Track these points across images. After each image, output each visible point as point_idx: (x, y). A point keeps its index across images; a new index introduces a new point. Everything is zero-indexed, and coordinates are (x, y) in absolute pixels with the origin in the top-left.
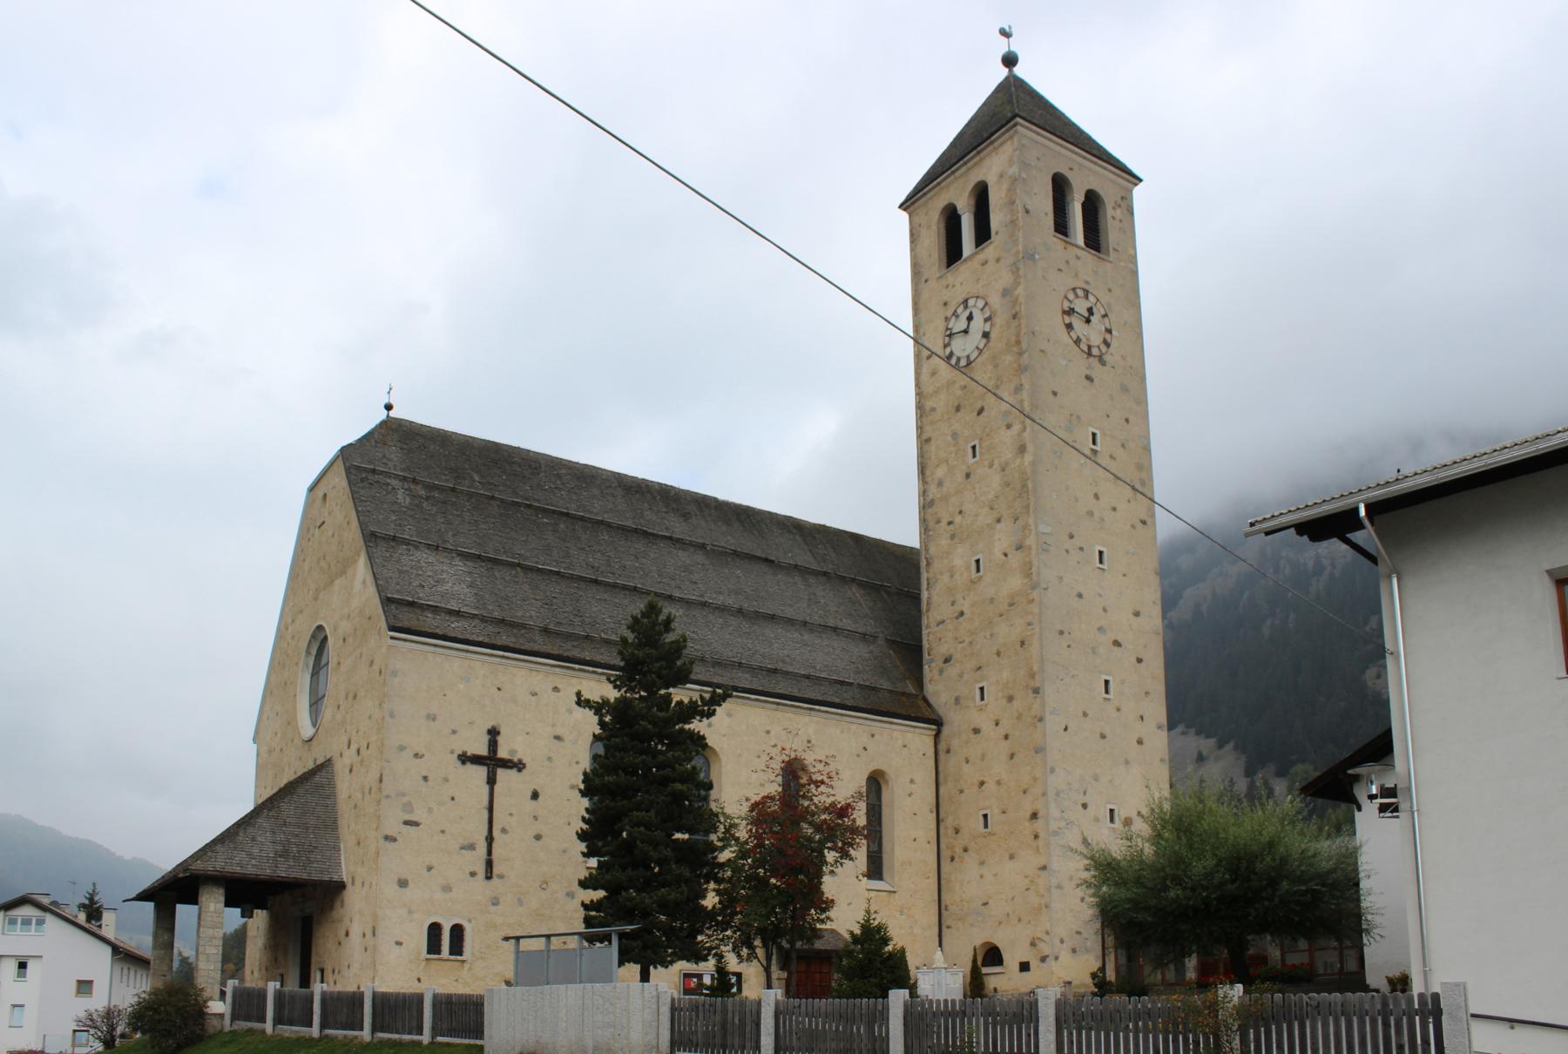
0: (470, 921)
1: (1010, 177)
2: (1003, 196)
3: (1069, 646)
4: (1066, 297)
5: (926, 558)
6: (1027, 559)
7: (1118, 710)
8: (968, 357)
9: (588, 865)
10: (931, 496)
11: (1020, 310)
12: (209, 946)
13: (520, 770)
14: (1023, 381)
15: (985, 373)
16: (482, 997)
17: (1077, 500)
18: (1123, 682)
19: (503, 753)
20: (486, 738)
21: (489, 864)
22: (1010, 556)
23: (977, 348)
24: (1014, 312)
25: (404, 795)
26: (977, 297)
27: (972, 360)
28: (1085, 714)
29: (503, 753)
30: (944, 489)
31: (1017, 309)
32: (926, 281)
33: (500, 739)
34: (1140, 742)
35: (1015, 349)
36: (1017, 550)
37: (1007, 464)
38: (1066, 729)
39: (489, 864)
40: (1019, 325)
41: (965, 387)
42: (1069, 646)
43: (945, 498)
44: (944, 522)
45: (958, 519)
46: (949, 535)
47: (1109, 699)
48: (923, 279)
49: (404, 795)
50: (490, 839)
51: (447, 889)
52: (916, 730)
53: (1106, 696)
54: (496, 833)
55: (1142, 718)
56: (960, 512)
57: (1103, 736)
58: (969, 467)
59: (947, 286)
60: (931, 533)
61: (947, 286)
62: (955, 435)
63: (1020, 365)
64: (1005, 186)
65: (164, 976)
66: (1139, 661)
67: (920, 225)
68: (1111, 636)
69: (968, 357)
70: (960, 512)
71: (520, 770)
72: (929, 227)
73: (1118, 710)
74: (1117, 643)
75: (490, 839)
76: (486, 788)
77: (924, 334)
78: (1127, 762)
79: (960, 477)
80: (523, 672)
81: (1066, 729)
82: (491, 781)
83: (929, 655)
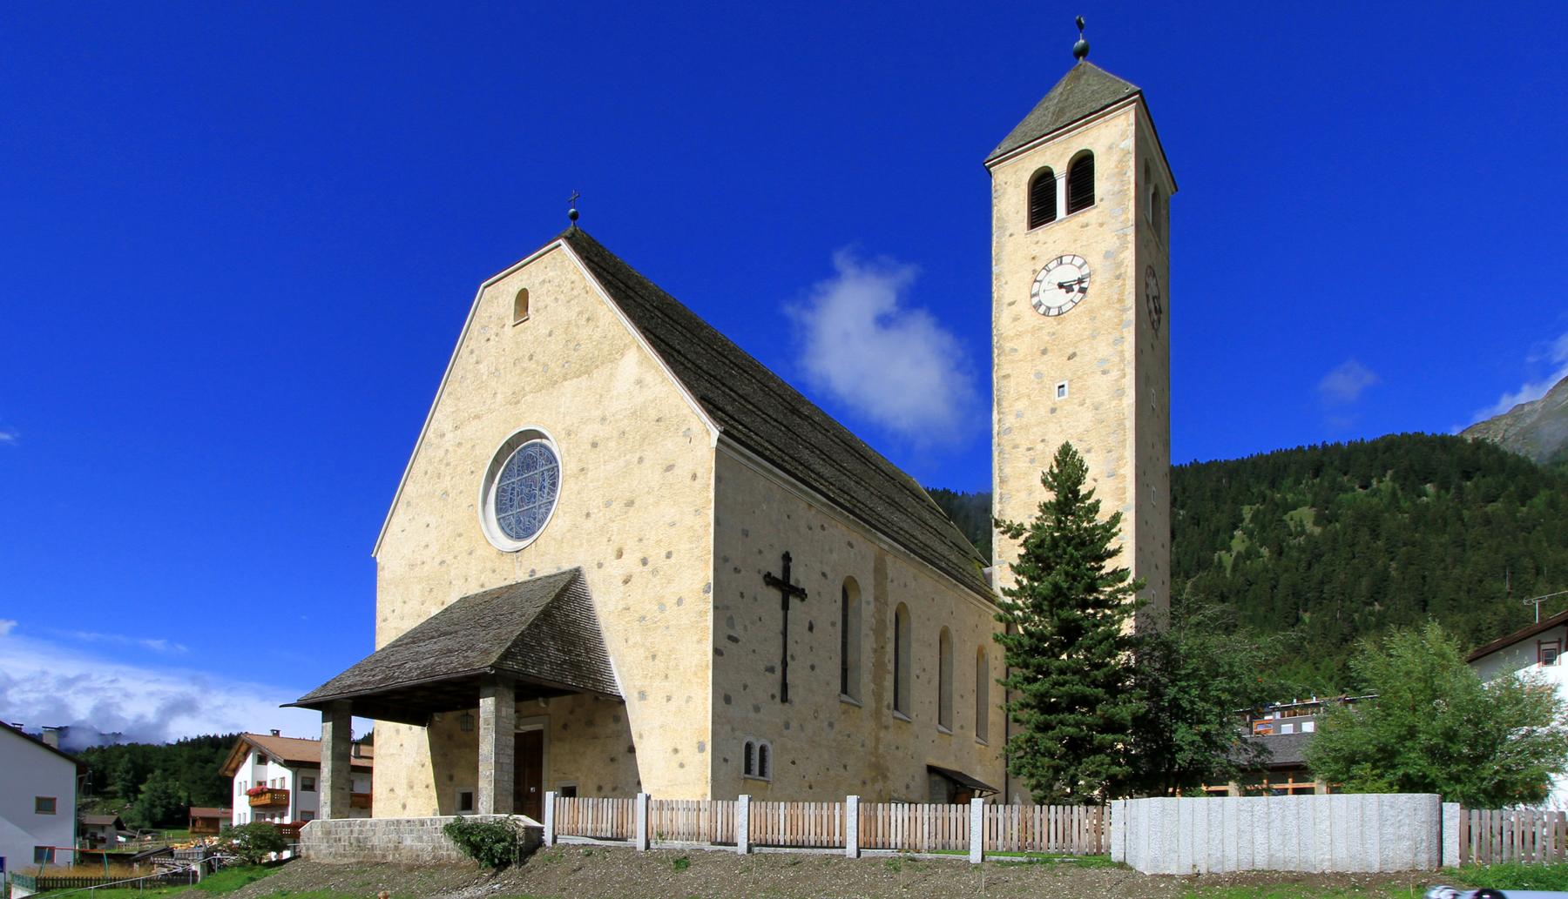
0: (772, 743)
1: (1123, 149)
2: (1113, 166)
5: (1000, 477)
6: (1121, 485)
8: (1049, 308)
9: (842, 699)
10: (1008, 425)
11: (1126, 272)
12: (503, 754)
14: (1125, 334)
15: (1079, 323)
16: (36, 813)
20: (780, 563)
21: (785, 687)
22: (1100, 481)
24: (1118, 273)
25: (728, 608)
26: (1074, 256)
27: (1064, 311)
30: (1024, 420)
31: (1123, 270)
32: (1011, 235)
35: (1117, 306)
36: (1108, 477)
37: (1101, 404)
39: (785, 687)
40: (1124, 285)
41: (1054, 334)
43: (1026, 428)
44: (1022, 449)
45: (1040, 446)
46: (1028, 459)
48: (1008, 233)
49: (728, 608)
50: (785, 664)
51: (757, 709)
54: (788, 659)
56: (1043, 441)
58: (1055, 403)
59: (1037, 242)
60: (1005, 456)
61: (1037, 242)
62: (1039, 375)
63: (1121, 321)
64: (1115, 158)
65: (343, 789)
67: (1006, 183)
69: (1060, 307)
70: (1043, 441)
72: (1017, 186)
75: (785, 664)
76: (780, 614)
77: (1006, 283)
79: (1043, 411)
82: (785, 606)
83: (1000, 556)
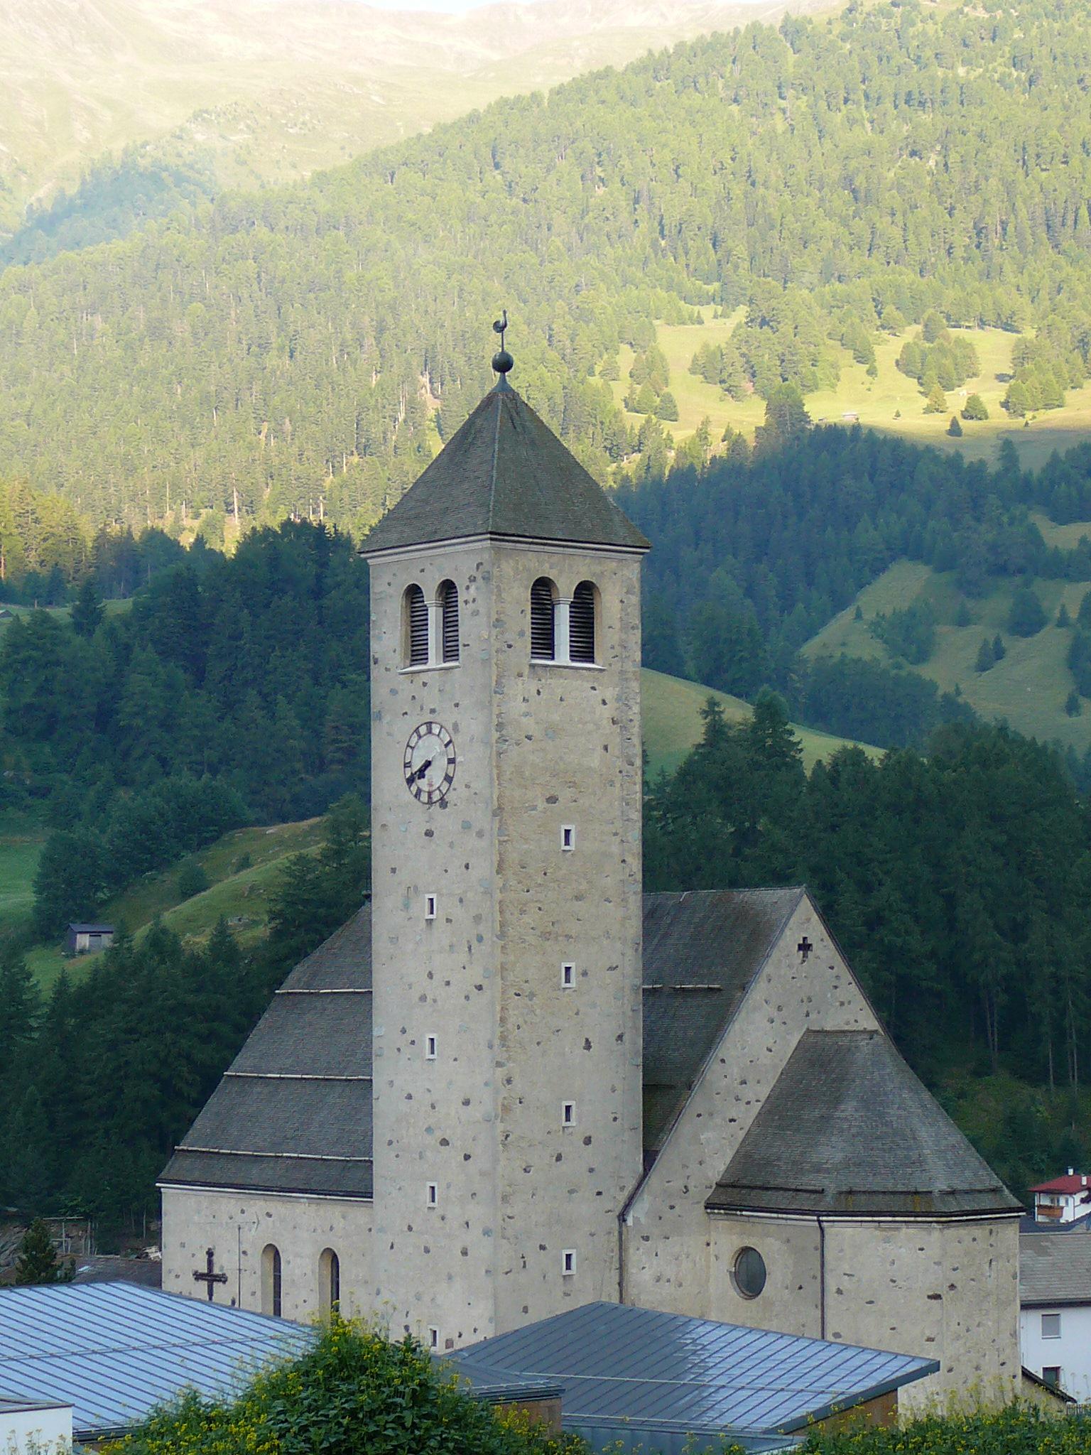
3: (397, 1156)
4: (417, 730)
7: (443, 1218)
13: (224, 1282)
17: (410, 986)
18: (449, 1186)
19: (216, 1271)
23: (412, 748)
28: (410, 1228)
29: (216, 1271)
33: (215, 1258)
34: (465, 1253)
38: (392, 1247)
42: (397, 1156)
47: (434, 1208)
52: (863, 1224)
53: (432, 1205)
55: (467, 1224)
57: (427, 1251)
66: (467, 1157)
68: (439, 1135)
69: (420, 737)
71: (224, 1282)
73: (443, 1218)
74: (445, 1142)
78: (450, 1277)
80: (225, 1200)
81: (392, 1247)
